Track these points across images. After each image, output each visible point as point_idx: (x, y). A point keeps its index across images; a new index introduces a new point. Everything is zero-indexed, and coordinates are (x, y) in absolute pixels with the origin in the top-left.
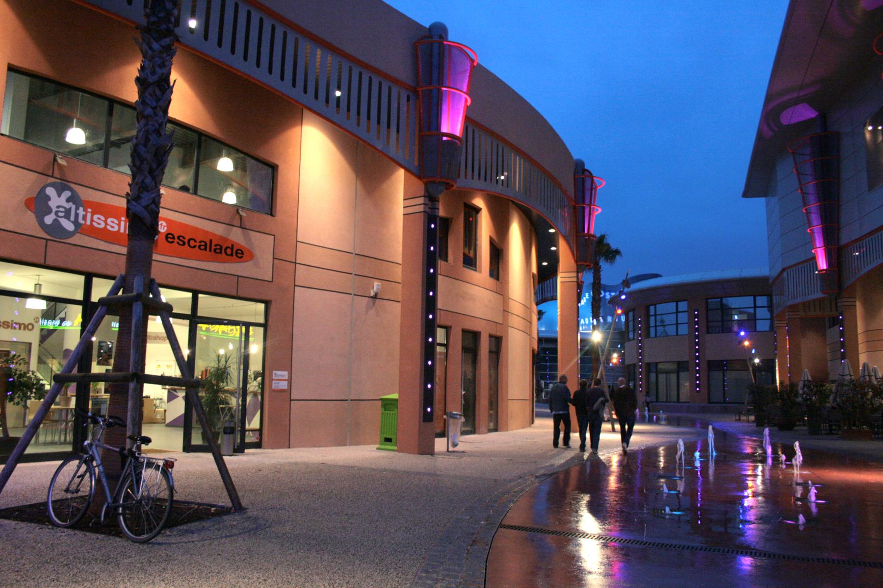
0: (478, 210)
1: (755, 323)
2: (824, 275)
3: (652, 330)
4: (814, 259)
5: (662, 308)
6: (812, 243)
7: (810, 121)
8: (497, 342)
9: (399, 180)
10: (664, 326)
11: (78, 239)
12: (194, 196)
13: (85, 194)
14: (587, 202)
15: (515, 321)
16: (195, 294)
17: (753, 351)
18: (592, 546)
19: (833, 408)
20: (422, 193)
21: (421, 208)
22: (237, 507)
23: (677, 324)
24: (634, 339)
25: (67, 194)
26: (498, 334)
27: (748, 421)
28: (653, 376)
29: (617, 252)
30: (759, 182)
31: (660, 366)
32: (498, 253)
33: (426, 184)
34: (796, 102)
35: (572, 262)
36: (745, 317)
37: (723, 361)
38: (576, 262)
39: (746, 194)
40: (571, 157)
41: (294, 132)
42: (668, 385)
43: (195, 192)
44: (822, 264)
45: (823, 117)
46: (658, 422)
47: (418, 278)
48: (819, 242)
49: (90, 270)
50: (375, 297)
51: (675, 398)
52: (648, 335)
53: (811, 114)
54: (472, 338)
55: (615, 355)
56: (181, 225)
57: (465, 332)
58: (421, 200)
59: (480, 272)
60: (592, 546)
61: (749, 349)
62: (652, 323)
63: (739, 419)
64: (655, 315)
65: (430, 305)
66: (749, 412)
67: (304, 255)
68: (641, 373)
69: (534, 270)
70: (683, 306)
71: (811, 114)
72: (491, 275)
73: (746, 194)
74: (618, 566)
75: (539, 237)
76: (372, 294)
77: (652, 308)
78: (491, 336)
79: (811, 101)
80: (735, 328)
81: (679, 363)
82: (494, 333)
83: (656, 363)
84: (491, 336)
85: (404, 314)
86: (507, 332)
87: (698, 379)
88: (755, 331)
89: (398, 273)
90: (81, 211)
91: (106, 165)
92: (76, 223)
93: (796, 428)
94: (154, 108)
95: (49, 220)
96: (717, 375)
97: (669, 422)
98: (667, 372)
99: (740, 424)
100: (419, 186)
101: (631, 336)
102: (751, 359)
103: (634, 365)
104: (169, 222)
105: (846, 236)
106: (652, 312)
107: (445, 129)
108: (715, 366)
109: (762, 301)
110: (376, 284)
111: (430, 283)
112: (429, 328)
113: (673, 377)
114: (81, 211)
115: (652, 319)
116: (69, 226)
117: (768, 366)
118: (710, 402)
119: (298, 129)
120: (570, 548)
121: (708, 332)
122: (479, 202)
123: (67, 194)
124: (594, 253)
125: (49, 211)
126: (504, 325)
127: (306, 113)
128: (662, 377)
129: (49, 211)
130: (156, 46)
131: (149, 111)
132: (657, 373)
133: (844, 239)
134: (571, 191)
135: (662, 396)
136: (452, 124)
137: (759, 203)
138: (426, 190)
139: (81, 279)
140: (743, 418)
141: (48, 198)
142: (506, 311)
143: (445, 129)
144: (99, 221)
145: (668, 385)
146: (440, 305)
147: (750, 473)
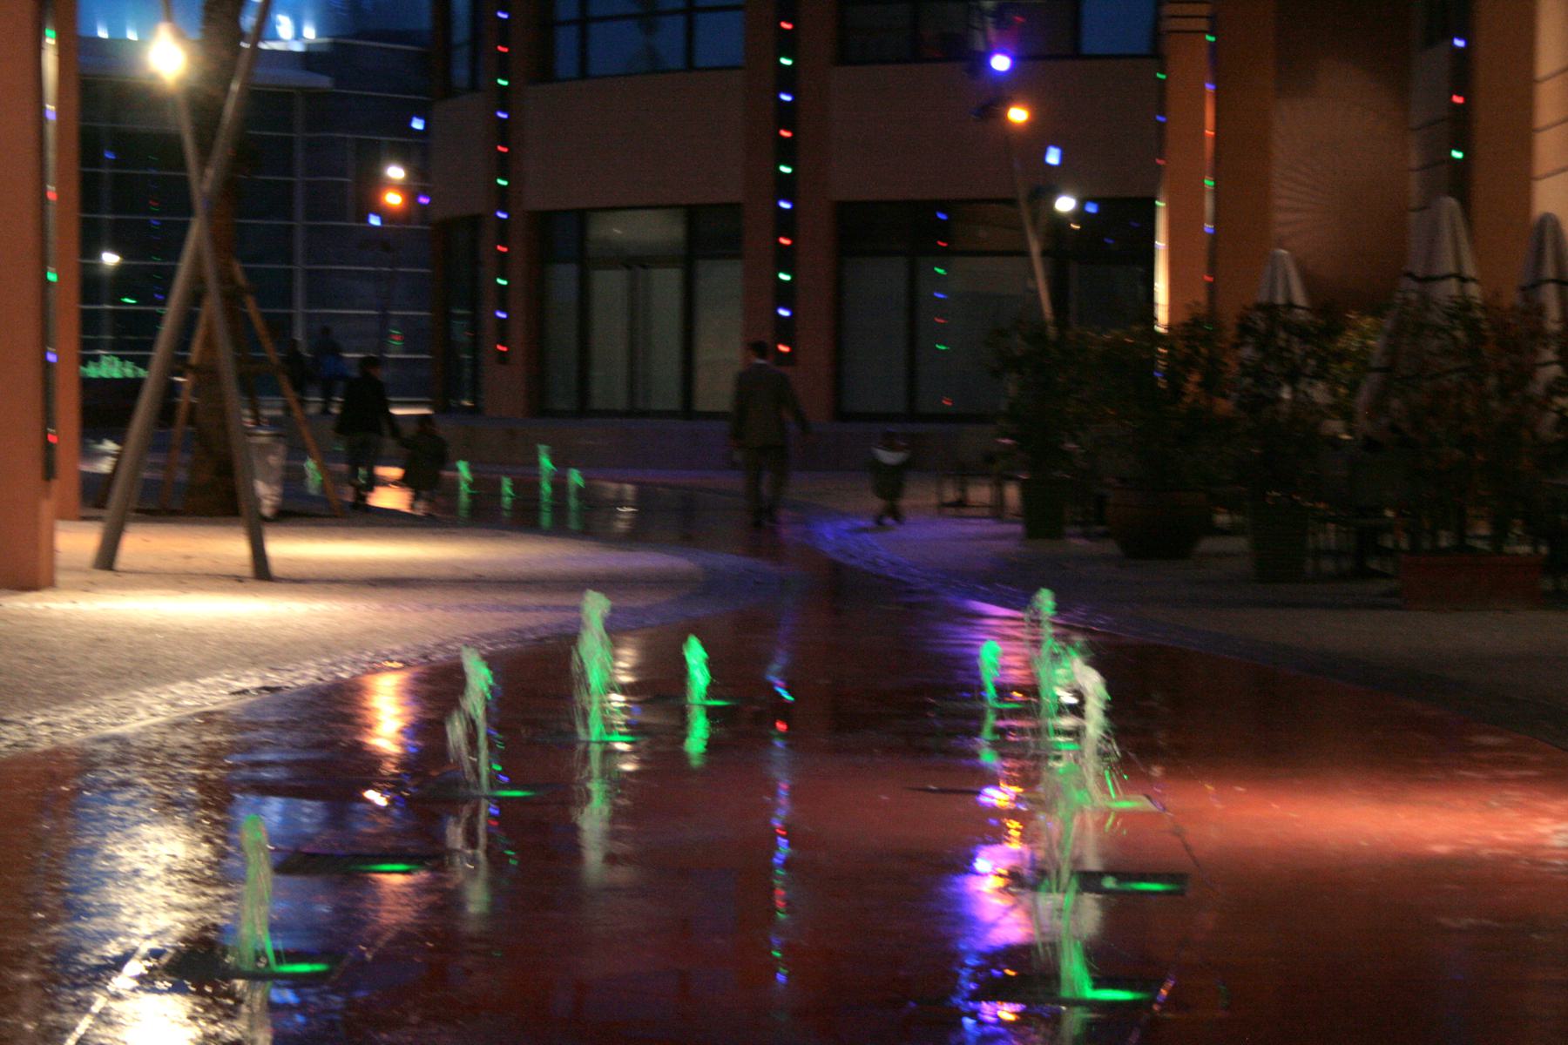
17: (1053, 157)
18: (1134, 1037)
19: (1371, 444)
24: (474, 87)
27: (997, 510)
51: (666, 395)
52: (544, 72)
55: (310, 465)
60: (1134, 1037)
63: (961, 503)
66: (990, 467)
83: (581, 217)
87: (784, 295)
93: (1207, 544)
96: (881, 278)
98: (636, 261)
99: (973, 528)
101: (461, 74)
103: (474, 223)
108: (864, 229)
113: (666, 283)
117: (1119, 237)
118: (841, 415)
120: (1035, 965)
121: (844, 57)
128: (609, 285)
135: (609, 386)
140: (980, 493)
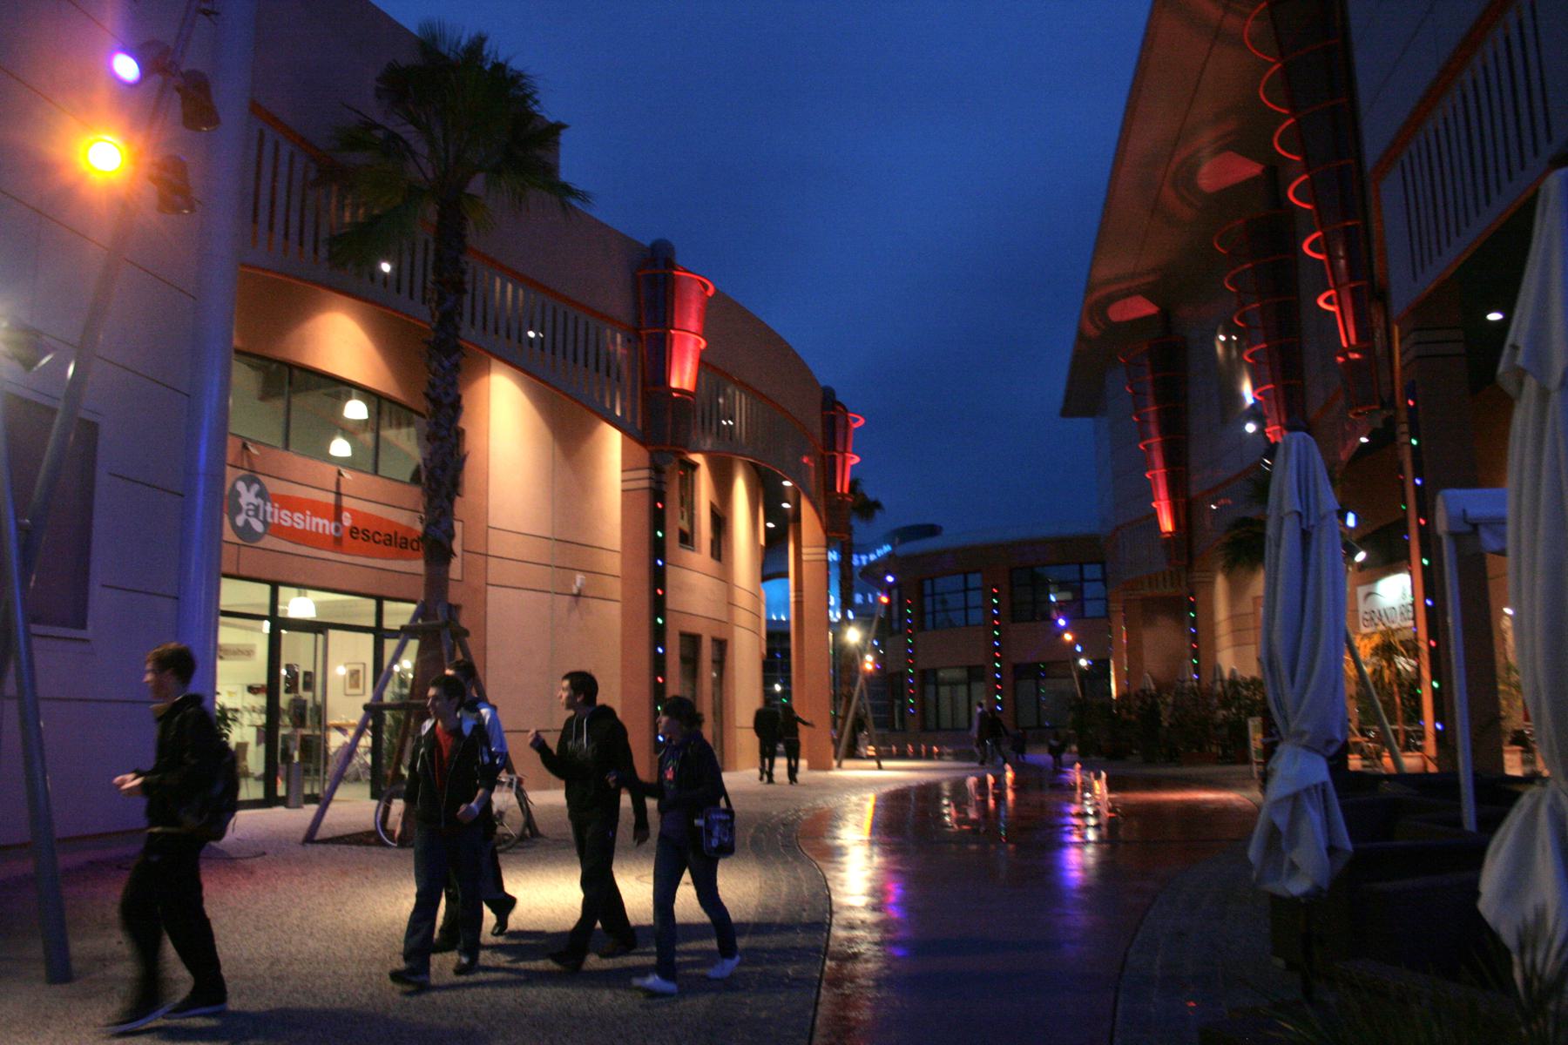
0: (695, 466)
1: (1082, 606)
2: (1170, 541)
3: (929, 618)
4: (1154, 517)
5: (942, 584)
6: (1150, 495)
7: (1146, 319)
8: (721, 646)
9: (611, 444)
10: (947, 611)
11: (269, 542)
12: (371, 478)
13: (274, 487)
14: (840, 449)
15: (743, 618)
16: (380, 600)
20: (647, 464)
21: (645, 483)
22: (535, 833)
23: (966, 608)
25: (256, 487)
26: (723, 636)
28: (931, 689)
29: (877, 505)
30: (1083, 397)
31: (941, 674)
32: (721, 522)
33: (651, 454)
34: (1129, 293)
35: (820, 532)
36: (1067, 596)
37: (1037, 664)
38: (826, 531)
39: (1066, 413)
40: (814, 381)
41: (480, 384)
42: (953, 701)
43: (376, 472)
44: (1167, 524)
45: (1165, 315)
46: (940, 756)
47: (643, 573)
48: (1162, 492)
49: (279, 578)
50: (578, 595)
53: (1149, 309)
54: (691, 642)
56: (368, 516)
57: (683, 634)
58: (645, 473)
59: (699, 552)
61: (1072, 645)
62: (929, 608)
64: (933, 595)
65: (658, 606)
67: (497, 545)
68: (911, 686)
69: (762, 541)
70: (975, 580)
71: (1149, 309)
72: (712, 555)
73: (1066, 413)
74: (895, 892)
75: (767, 495)
76: (575, 591)
77: (928, 583)
78: (714, 640)
79: (1150, 293)
80: (1054, 615)
81: (970, 669)
82: (717, 635)
84: (714, 640)
85: (624, 615)
86: (732, 633)
88: (1083, 617)
89: (614, 564)
90: (269, 508)
91: (287, 447)
92: (265, 522)
94: (448, 430)
95: (240, 520)
96: (1027, 685)
97: (957, 756)
98: (953, 684)
100: (642, 454)
102: (1076, 660)
104: (354, 513)
105: (1198, 483)
106: (928, 590)
107: (674, 384)
109: (1092, 571)
110: (579, 578)
111: (658, 578)
112: (658, 635)
113: (962, 691)
114: (269, 508)
115: (928, 601)
116: (258, 526)
117: (1100, 671)
119: (485, 380)
122: (698, 458)
123: (256, 487)
124: (846, 518)
125: (239, 510)
126: (729, 623)
127: (494, 362)
128: (944, 691)
129: (239, 510)
130: (446, 363)
131: (444, 433)
132: (937, 684)
133: (1194, 491)
134: (818, 430)
136: (683, 377)
137: (1084, 425)
138: (651, 457)
139: (372, 603)
141: (238, 495)
142: (731, 604)
143: (674, 384)
144: (300, 521)
145: (953, 701)
146: (670, 604)
147: (1076, 838)
